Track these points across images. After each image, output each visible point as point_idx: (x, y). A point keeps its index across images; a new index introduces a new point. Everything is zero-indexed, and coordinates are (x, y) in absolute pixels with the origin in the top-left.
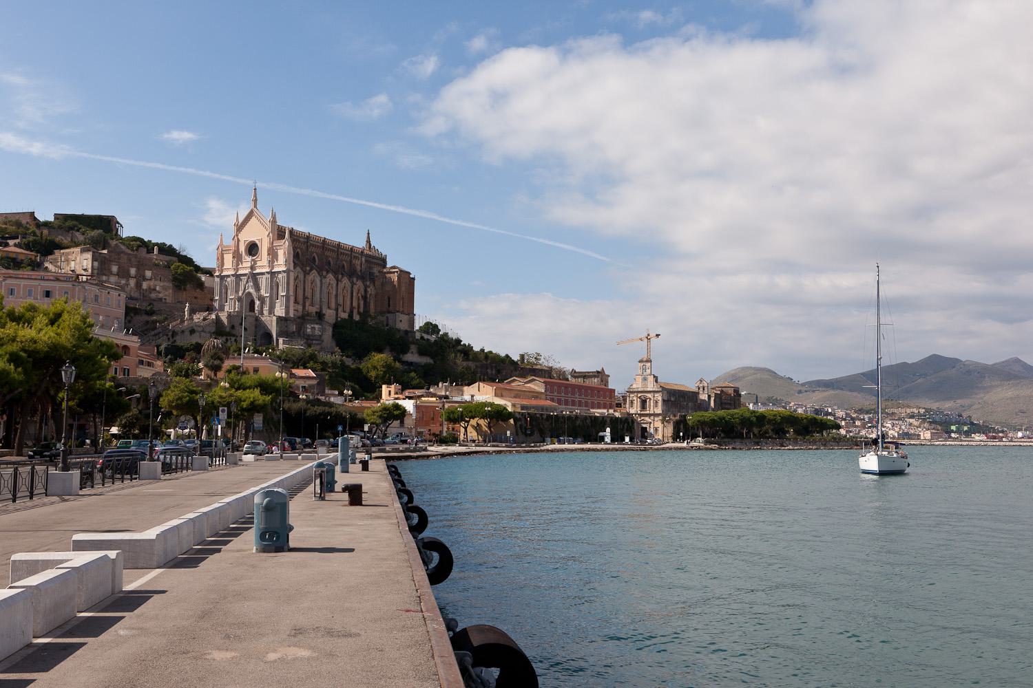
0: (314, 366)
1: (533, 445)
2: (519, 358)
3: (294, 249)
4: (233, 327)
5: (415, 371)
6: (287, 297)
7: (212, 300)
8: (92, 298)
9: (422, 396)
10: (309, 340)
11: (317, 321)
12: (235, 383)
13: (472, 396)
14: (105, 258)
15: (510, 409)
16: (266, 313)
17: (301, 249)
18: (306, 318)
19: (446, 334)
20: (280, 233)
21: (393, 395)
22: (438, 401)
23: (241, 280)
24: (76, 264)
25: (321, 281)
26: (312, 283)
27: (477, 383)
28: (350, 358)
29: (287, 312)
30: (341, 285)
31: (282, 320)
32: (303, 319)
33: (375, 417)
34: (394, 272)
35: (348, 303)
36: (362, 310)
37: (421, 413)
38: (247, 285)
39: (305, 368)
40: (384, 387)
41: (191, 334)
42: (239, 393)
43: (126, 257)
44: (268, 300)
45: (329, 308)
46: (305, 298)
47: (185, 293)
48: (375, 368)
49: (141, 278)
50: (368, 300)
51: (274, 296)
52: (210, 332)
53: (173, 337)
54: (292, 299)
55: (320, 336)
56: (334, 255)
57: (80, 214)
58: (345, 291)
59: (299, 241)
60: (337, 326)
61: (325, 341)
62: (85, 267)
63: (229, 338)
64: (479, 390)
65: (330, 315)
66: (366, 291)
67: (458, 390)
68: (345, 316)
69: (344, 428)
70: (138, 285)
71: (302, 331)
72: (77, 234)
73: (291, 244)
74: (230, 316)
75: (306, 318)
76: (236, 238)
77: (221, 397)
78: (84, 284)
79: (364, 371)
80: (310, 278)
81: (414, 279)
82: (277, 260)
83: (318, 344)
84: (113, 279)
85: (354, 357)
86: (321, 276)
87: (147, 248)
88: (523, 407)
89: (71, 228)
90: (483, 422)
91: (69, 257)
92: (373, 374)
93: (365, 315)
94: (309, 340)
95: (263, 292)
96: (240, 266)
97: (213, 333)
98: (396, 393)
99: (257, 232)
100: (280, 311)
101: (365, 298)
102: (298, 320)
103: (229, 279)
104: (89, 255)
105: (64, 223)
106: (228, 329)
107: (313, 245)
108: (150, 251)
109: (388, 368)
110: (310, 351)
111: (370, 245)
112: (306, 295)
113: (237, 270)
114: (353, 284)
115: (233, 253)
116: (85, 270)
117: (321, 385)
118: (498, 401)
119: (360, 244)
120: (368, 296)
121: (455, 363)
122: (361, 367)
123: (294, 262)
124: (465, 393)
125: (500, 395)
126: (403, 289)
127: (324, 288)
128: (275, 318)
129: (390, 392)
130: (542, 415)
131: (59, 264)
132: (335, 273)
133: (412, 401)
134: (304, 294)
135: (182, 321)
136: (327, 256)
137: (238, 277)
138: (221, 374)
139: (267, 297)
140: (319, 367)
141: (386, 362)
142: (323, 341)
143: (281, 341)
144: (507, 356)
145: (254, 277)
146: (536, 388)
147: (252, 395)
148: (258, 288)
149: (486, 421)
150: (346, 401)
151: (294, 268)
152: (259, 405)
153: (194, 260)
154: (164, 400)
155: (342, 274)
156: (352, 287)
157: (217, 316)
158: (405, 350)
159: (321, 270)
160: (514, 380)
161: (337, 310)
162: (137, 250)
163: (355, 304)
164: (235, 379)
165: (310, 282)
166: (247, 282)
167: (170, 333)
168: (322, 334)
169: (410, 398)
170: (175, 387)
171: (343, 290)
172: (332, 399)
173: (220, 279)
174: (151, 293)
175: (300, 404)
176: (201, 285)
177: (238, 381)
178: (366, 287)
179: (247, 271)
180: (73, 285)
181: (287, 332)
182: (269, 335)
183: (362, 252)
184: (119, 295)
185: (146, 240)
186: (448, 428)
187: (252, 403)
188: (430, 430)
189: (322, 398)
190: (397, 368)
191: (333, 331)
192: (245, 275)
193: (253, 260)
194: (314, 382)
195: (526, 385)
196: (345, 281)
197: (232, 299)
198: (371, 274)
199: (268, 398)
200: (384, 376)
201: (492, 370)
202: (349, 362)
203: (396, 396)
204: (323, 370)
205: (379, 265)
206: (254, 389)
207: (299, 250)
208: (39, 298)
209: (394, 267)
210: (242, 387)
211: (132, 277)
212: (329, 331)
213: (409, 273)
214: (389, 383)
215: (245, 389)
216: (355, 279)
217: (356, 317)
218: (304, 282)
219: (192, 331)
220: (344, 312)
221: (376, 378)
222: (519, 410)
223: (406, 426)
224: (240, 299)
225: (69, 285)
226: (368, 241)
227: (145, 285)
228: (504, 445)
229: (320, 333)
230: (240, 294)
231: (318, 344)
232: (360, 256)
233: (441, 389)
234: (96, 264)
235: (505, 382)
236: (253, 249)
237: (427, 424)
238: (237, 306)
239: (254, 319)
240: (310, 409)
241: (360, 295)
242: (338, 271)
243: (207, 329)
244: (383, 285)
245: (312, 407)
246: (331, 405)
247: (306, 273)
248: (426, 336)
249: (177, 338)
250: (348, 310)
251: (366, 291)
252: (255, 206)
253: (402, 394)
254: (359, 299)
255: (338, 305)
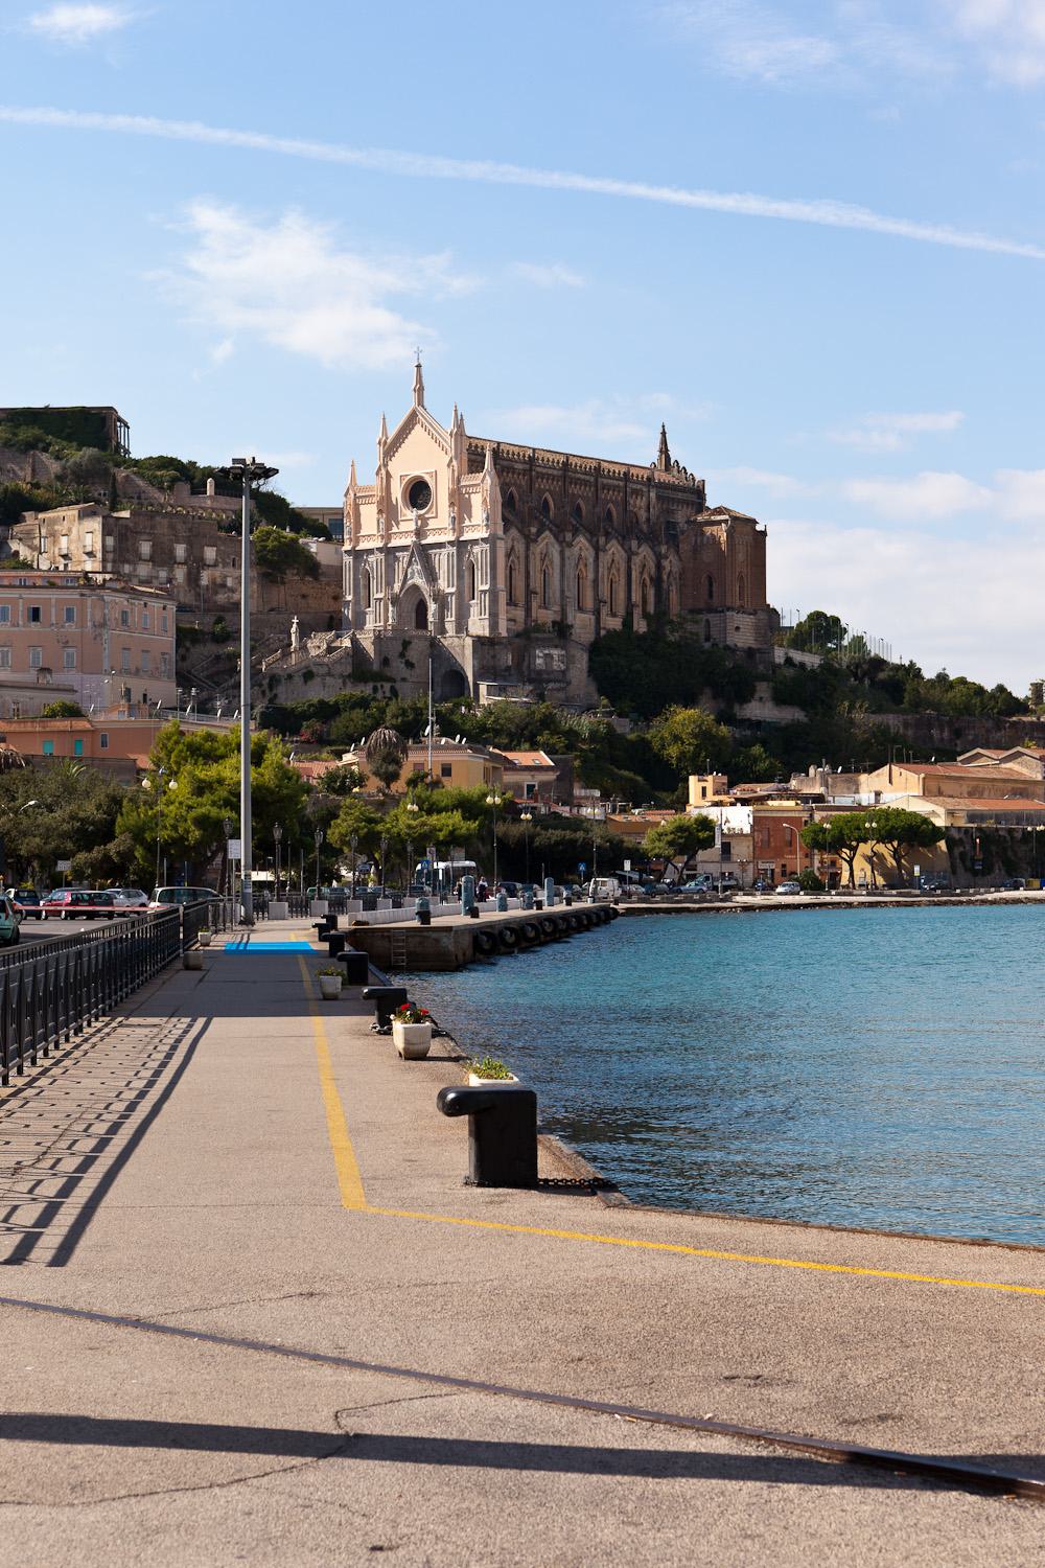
0: (551, 741)
1: (958, 891)
2: (1029, 693)
3: (504, 488)
4: (386, 662)
5: (764, 743)
6: (493, 593)
7: (338, 597)
8: (116, 619)
9: (769, 797)
10: (538, 682)
11: (557, 642)
12: (424, 803)
13: (878, 794)
14: (126, 526)
15: (940, 822)
16: (450, 627)
17: (518, 487)
18: (533, 635)
19: (859, 642)
20: (473, 456)
21: (710, 796)
22: (800, 808)
23: (397, 559)
24: (69, 542)
25: (562, 553)
26: (543, 560)
27: (886, 768)
28: (627, 717)
29: (494, 626)
30: (605, 559)
31: (483, 644)
32: (527, 637)
33: (662, 844)
34: (719, 523)
35: (621, 595)
36: (651, 609)
37: (765, 833)
38: (410, 570)
39: (534, 747)
40: (693, 779)
41: (306, 682)
42: (434, 820)
43: (165, 522)
44: (453, 601)
45: (580, 609)
46: (529, 592)
47: (282, 587)
48: (677, 738)
49: (196, 564)
50: (665, 586)
51: (466, 592)
52: (341, 676)
53: (271, 687)
54: (503, 597)
55: (563, 672)
56: (589, 492)
57: (41, 405)
58: (614, 571)
59: (514, 470)
60: (596, 649)
61: (575, 682)
62: (89, 549)
63: (379, 685)
64: (890, 782)
65: (582, 625)
66: (659, 567)
67: (848, 781)
68: (614, 624)
69: (589, 866)
70: (193, 579)
71: (526, 664)
72: (44, 457)
73: (496, 480)
74: (379, 639)
75: (533, 635)
76: (383, 471)
77: (409, 827)
78: (102, 592)
79: (656, 745)
80: (538, 549)
81: (764, 534)
82: (470, 517)
83: (558, 690)
84: (144, 570)
85: (634, 716)
86: (561, 543)
87: (192, 484)
88: (972, 817)
89: (30, 446)
90: (884, 849)
91: (56, 527)
92: (673, 751)
93: (658, 619)
94: (538, 682)
95: (442, 584)
96: (395, 530)
97: (349, 676)
98: (716, 793)
99: (426, 458)
100: (479, 625)
101: (657, 581)
102: (517, 640)
103: (372, 558)
104: (96, 524)
105: (15, 434)
106: (376, 667)
107: (542, 476)
108: (198, 489)
109: (704, 737)
110: (542, 708)
111: (668, 458)
112: (531, 587)
113: (388, 537)
114: (630, 554)
115: (380, 503)
116: (90, 554)
117: (565, 777)
118: (922, 807)
119: (644, 456)
120: (665, 577)
121: (852, 722)
122: (648, 736)
123: (504, 519)
124: (864, 788)
125: (935, 790)
126: (741, 557)
127: (571, 572)
128: (469, 641)
129: (704, 789)
130: (1010, 831)
131: (36, 542)
132: (592, 534)
133: (748, 809)
134: (527, 585)
135: (286, 654)
136: (573, 494)
137: (390, 552)
138: (399, 786)
139: (452, 594)
140: (559, 742)
141: (700, 726)
142: (569, 683)
143: (483, 688)
144: (1001, 689)
145: (423, 553)
146: (1024, 771)
147: (451, 822)
148: (431, 575)
149: (889, 846)
150: (614, 811)
151: (504, 533)
152: (461, 836)
153: (289, 500)
154: (333, 833)
155: (607, 534)
156: (629, 560)
157: (354, 641)
158: (745, 695)
159: (563, 531)
160: (978, 756)
161: (597, 613)
162: (171, 488)
163: (636, 597)
164: (423, 796)
165: (538, 558)
166: (410, 563)
167: (266, 682)
168: (568, 668)
169: (745, 802)
170: (347, 814)
171: (609, 569)
172: (587, 812)
173: (355, 559)
174: (216, 593)
175: (522, 828)
176: (311, 567)
177: (428, 798)
178: (659, 557)
179: (408, 541)
180: (82, 595)
181: (494, 668)
182: (458, 676)
183: (649, 479)
184: (164, 608)
185: (185, 461)
186: (822, 862)
187: (452, 833)
188: (784, 866)
189: (565, 811)
190: (723, 738)
191: (590, 660)
192: (404, 548)
193: (419, 517)
194: (551, 777)
195: (1003, 766)
196: (614, 549)
197: (380, 599)
198: (671, 525)
199: (474, 825)
200: (696, 755)
201: (942, 731)
202: (623, 726)
203: (717, 798)
204: (570, 748)
205: (687, 503)
206: (452, 810)
207: (513, 489)
208: (21, 623)
209: (719, 511)
210: (432, 809)
211: (179, 563)
212: (582, 661)
213: (755, 522)
214: (701, 772)
215: (439, 812)
216: (634, 544)
217: (640, 626)
218: (527, 557)
219: (308, 676)
220: (614, 615)
221: (679, 759)
222: (962, 823)
223: (734, 858)
224: (395, 600)
225: (74, 595)
226: (664, 451)
227: (205, 578)
228: (894, 892)
229: (563, 667)
230: (397, 587)
231: (558, 690)
232: (645, 489)
233: (811, 782)
234: (110, 541)
235: (959, 759)
236: (418, 492)
237: (779, 854)
238: (390, 615)
239: (427, 643)
240: (539, 835)
241: (646, 576)
242: (600, 528)
243: (338, 669)
244: (696, 550)
245: (543, 832)
246: (577, 824)
247: (530, 540)
248: (797, 656)
249: (281, 690)
250: (621, 610)
251: (659, 567)
252: (421, 402)
253: (728, 793)
254: (644, 585)
255: (598, 601)
